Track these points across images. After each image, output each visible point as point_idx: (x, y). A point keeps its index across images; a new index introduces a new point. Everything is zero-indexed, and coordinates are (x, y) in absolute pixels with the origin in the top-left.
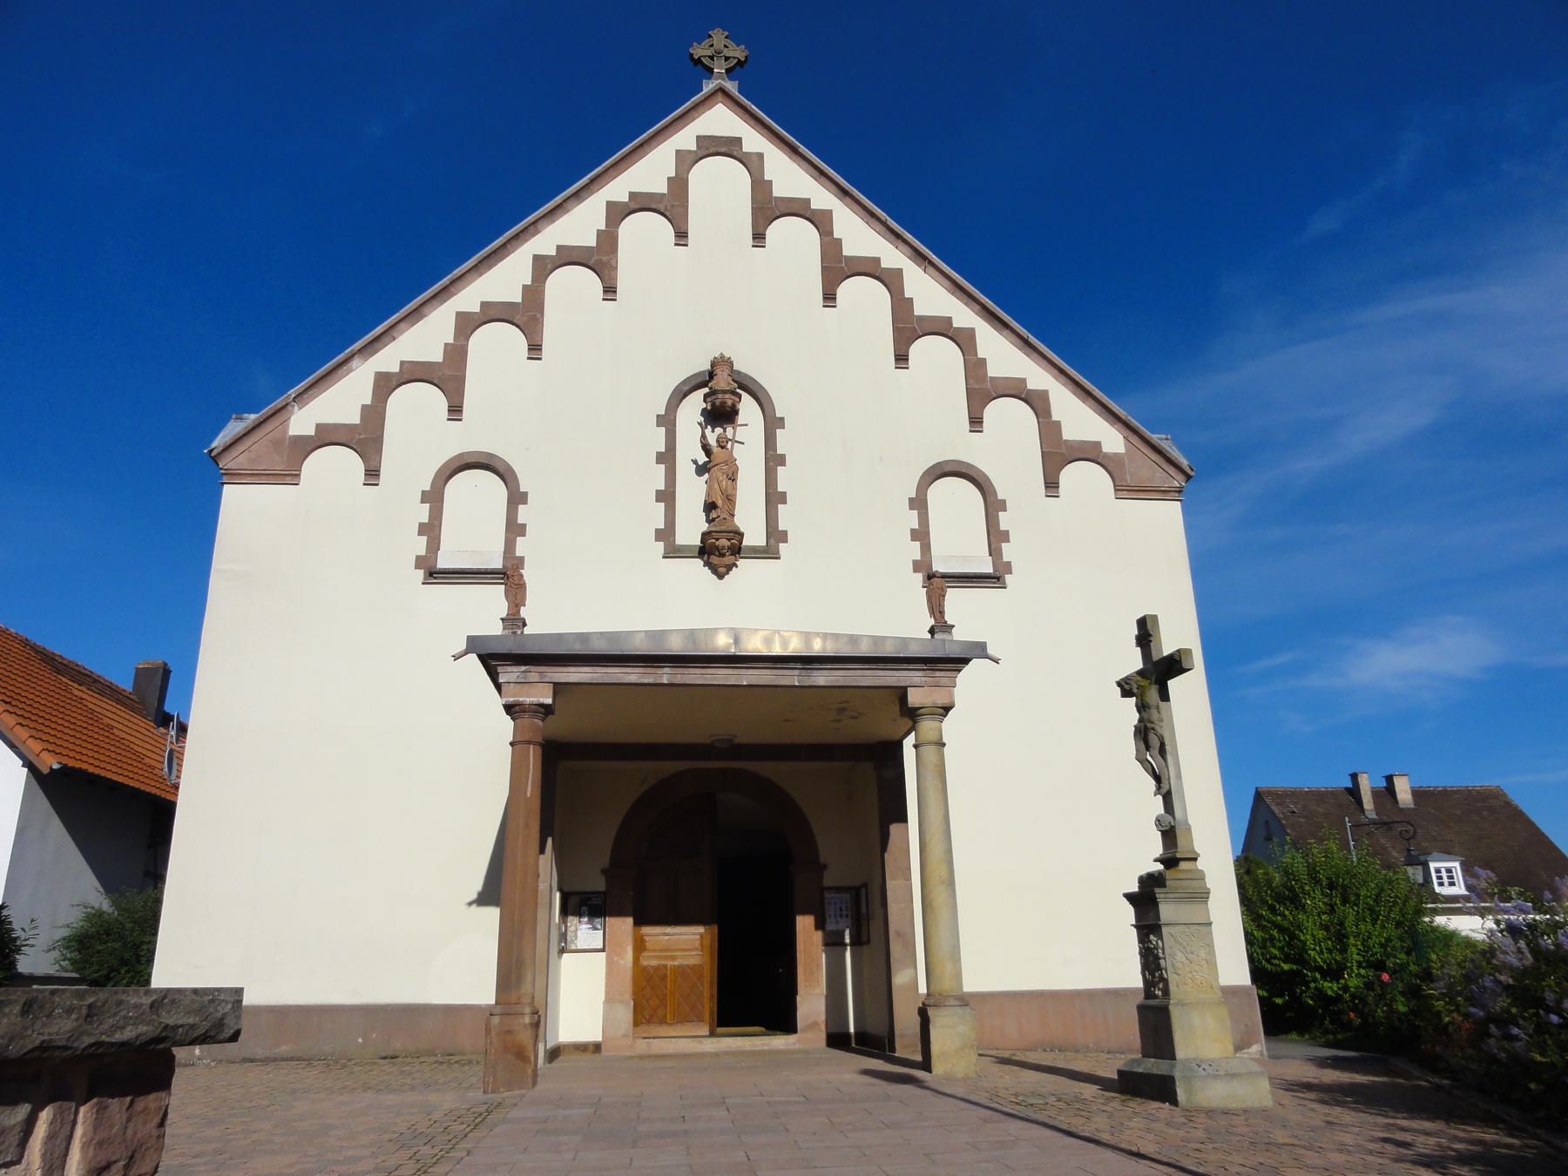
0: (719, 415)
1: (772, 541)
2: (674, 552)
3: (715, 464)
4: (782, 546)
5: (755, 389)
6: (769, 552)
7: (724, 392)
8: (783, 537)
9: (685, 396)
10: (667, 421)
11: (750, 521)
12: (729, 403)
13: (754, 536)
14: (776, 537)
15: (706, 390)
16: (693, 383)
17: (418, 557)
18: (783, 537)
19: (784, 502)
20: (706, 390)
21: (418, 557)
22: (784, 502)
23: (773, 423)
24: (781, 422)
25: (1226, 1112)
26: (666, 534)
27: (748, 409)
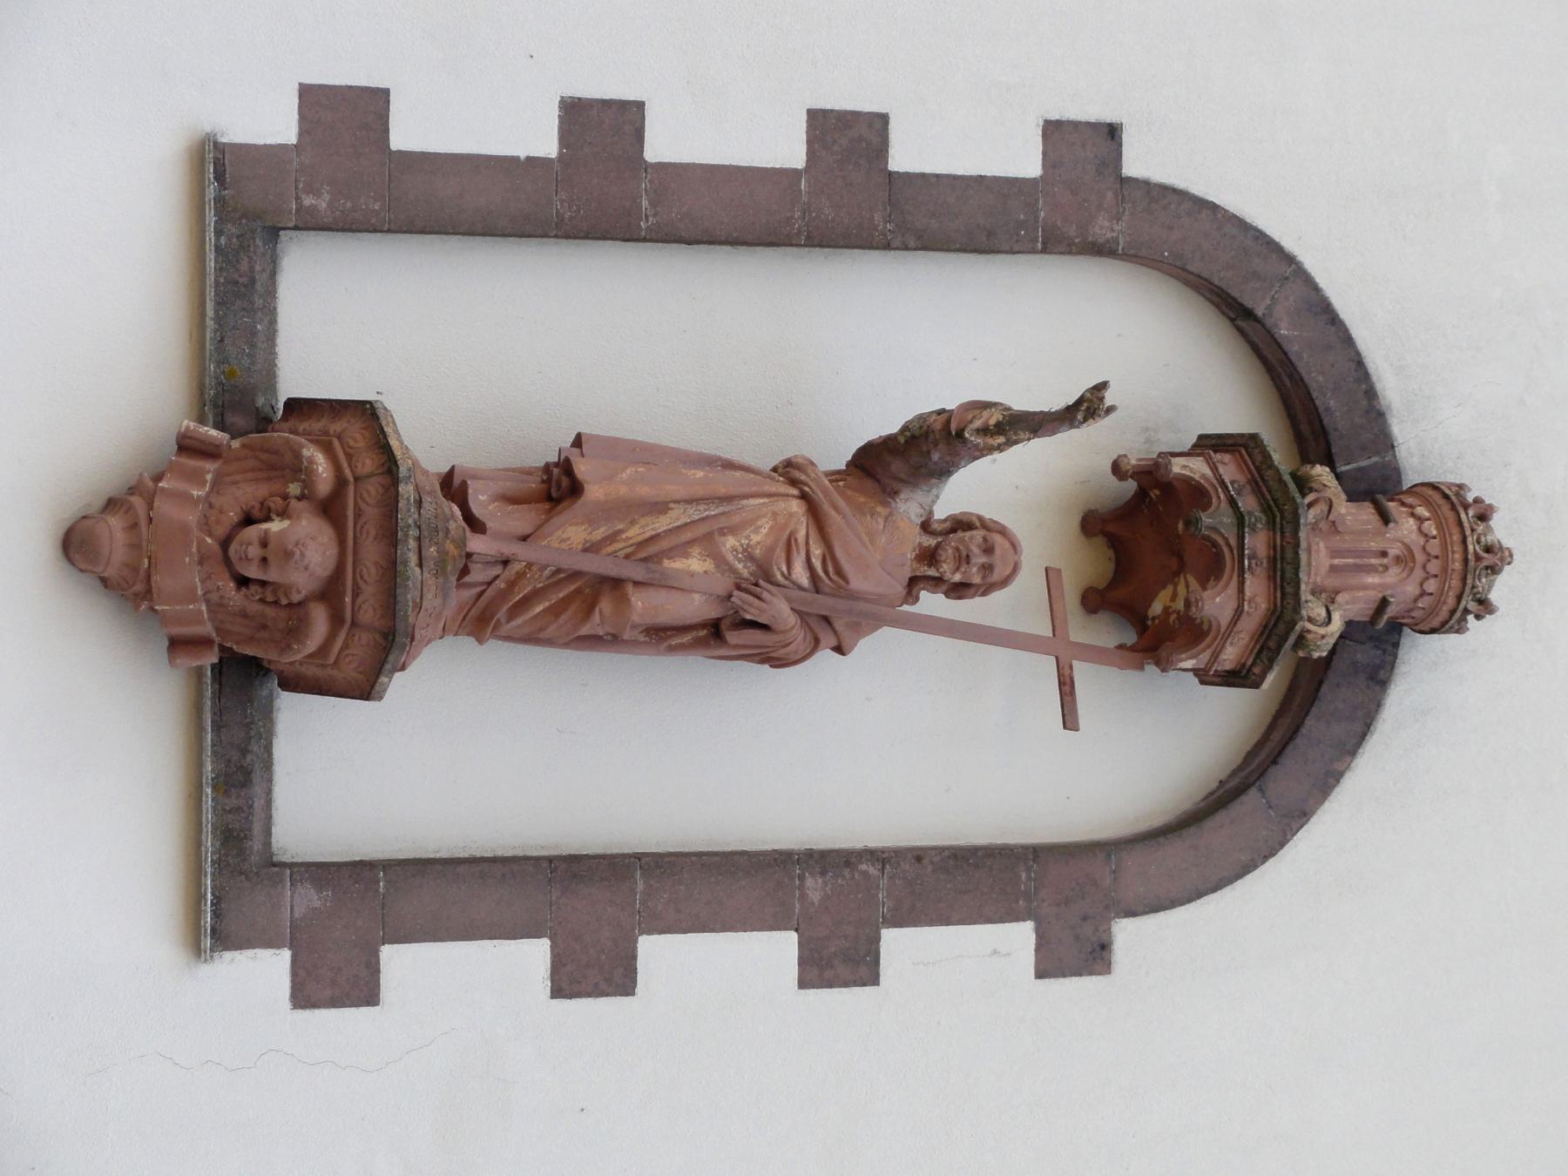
0: (1150, 559)
1: (306, 899)
2: (244, 216)
3: (847, 544)
4: (270, 969)
5: (1284, 781)
6: (238, 880)
7: (1284, 571)
8: (335, 977)
9: (1236, 313)
10: (1083, 201)
11: (409, 757)
12: (1216, 604)
13: (344, 774)
14: (329, 923)
15: (1281, 456)
16: (1316, 373)
17: (304, 996)
18: (335, 977)
19: (565, 984)
20: (1281, 456)
21: (304, 996)
22: (565, 984)
23: (1068, 898)
24: (1076, 952)
25: (556, 236)
26: (328, 175)
27: (1153, 740)
